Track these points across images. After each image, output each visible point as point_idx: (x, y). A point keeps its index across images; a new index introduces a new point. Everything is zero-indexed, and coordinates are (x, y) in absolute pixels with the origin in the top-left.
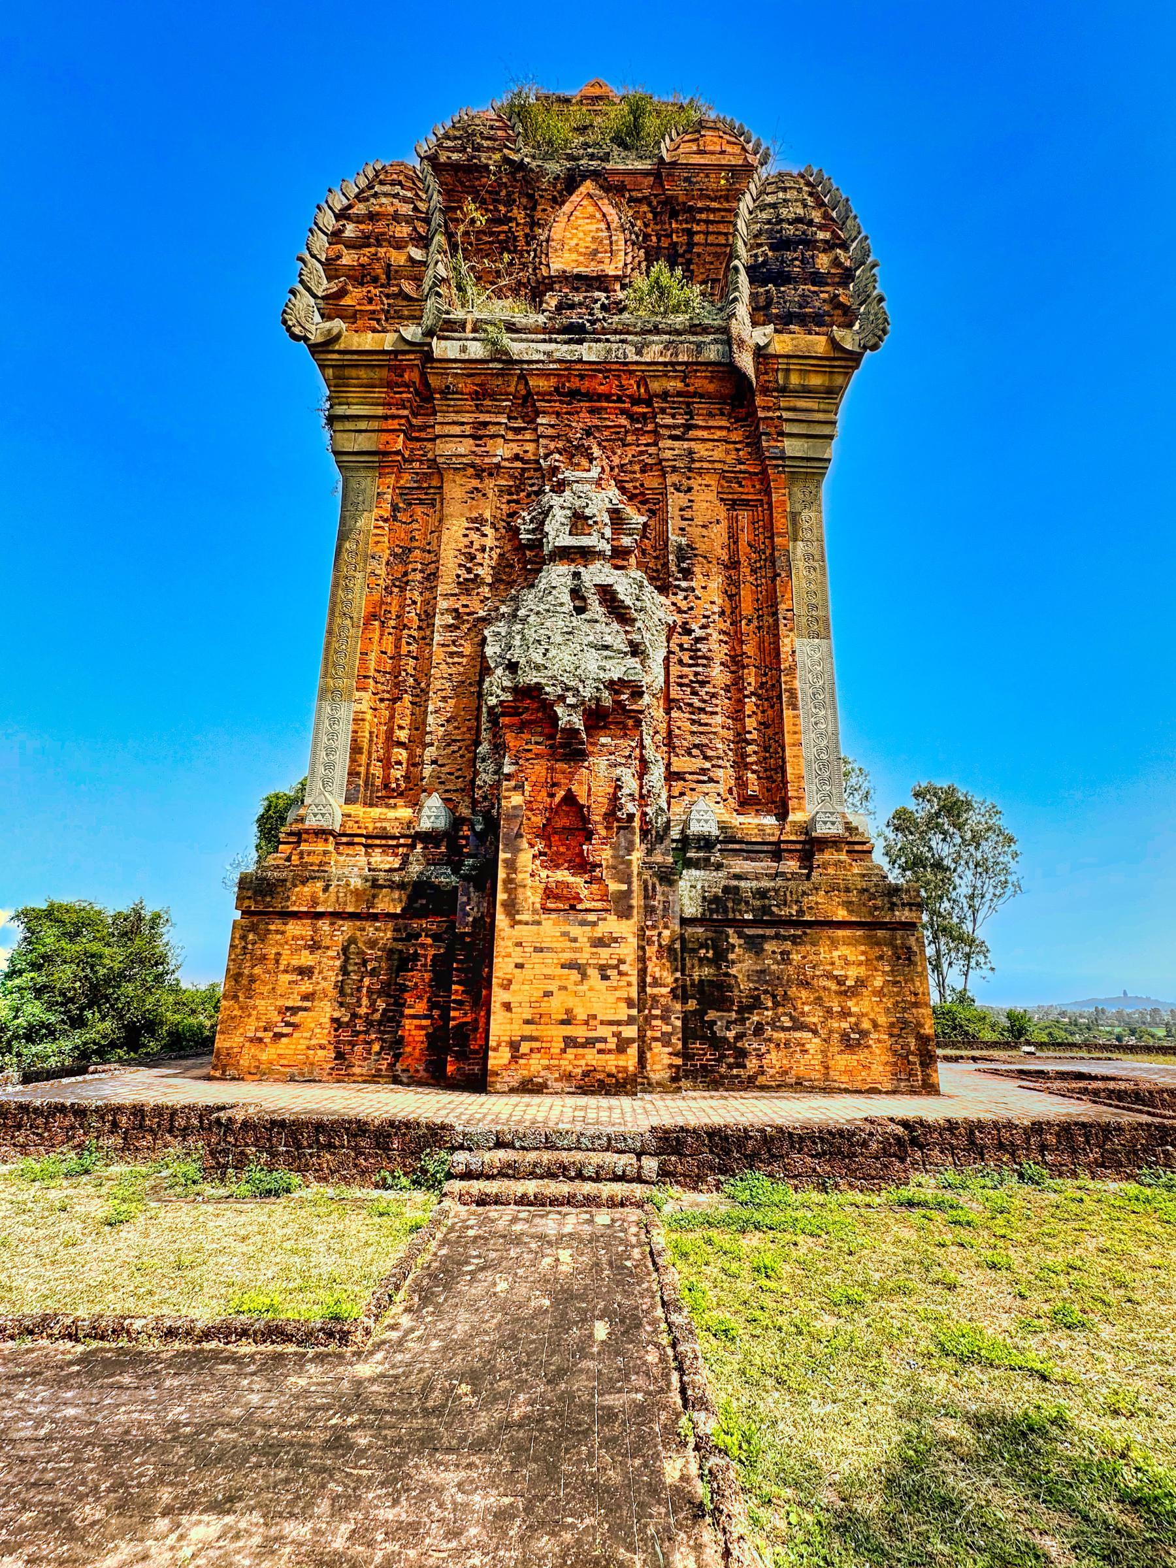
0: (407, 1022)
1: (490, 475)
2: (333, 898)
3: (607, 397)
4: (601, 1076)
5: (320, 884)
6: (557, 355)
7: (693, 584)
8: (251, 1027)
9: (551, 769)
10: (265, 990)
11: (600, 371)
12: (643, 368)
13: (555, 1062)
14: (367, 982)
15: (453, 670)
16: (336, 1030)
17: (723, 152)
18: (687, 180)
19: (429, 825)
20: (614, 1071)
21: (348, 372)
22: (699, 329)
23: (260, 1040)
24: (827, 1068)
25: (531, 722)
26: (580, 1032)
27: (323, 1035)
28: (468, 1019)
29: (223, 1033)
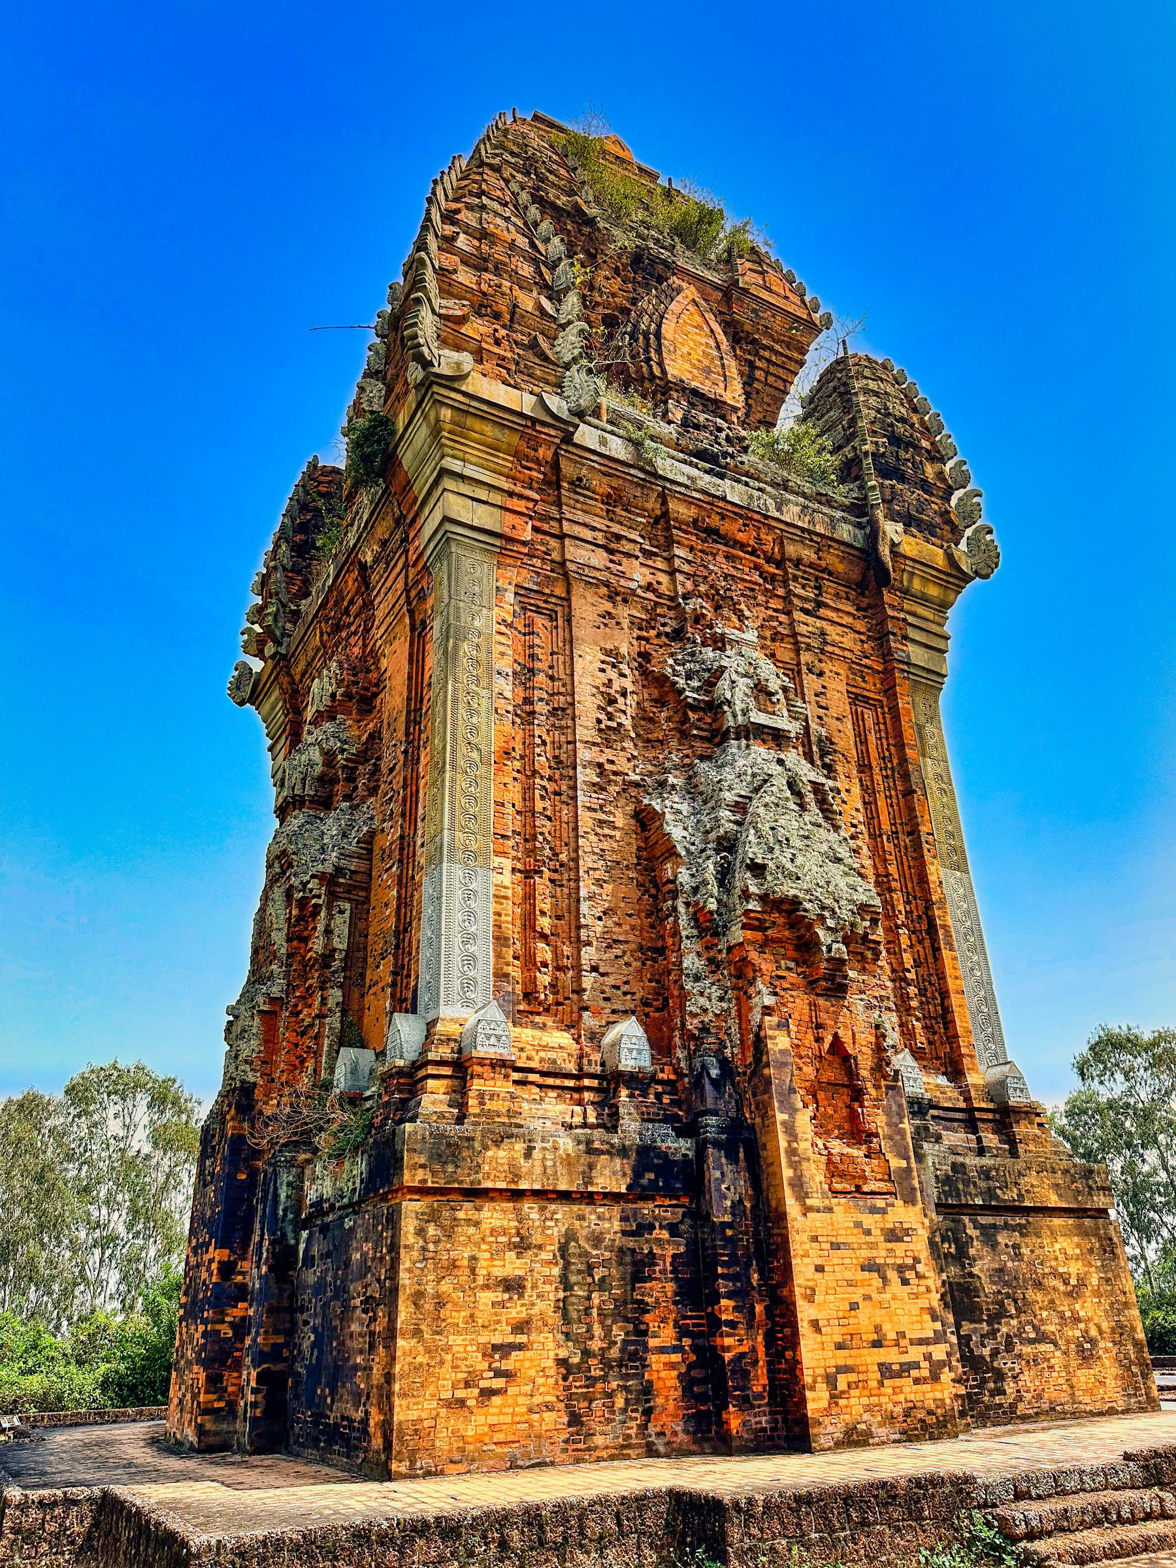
0: (653, 1358)
1: (625, 601)
2: (538, 1170)
3: (742, 546)
4: (921, 1415)
5: (520, 1147)
6: (700, 484)
7: (838, 785)
8: (446, 1382)
9: (813, 1005)
10: (460, 1317)
11: (741, 516)
12: (783, 527)
13: (874, 1400)
14: (596, 1298)
15: (605, 845)
16: (565, 1379)
17: (786, 298)
18: (754, 311)
19: (632, 1063)
20: (933, 1406)
21: (470, 421)
22: (824, 499)
23: (462, 1402)
24: (1072, 1387)
25: (774, 941)
26: (891, 1356)
27: (548, 1388)
28: (744, 1349)
29: (404, 1395)
